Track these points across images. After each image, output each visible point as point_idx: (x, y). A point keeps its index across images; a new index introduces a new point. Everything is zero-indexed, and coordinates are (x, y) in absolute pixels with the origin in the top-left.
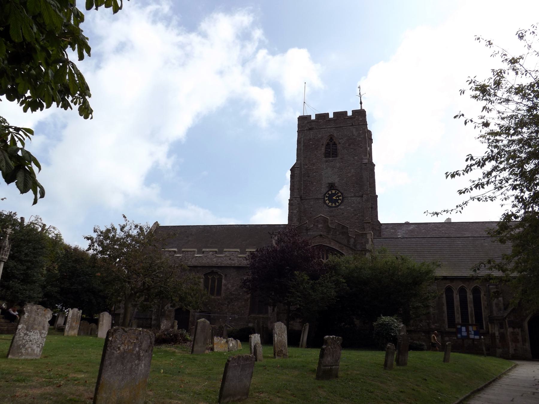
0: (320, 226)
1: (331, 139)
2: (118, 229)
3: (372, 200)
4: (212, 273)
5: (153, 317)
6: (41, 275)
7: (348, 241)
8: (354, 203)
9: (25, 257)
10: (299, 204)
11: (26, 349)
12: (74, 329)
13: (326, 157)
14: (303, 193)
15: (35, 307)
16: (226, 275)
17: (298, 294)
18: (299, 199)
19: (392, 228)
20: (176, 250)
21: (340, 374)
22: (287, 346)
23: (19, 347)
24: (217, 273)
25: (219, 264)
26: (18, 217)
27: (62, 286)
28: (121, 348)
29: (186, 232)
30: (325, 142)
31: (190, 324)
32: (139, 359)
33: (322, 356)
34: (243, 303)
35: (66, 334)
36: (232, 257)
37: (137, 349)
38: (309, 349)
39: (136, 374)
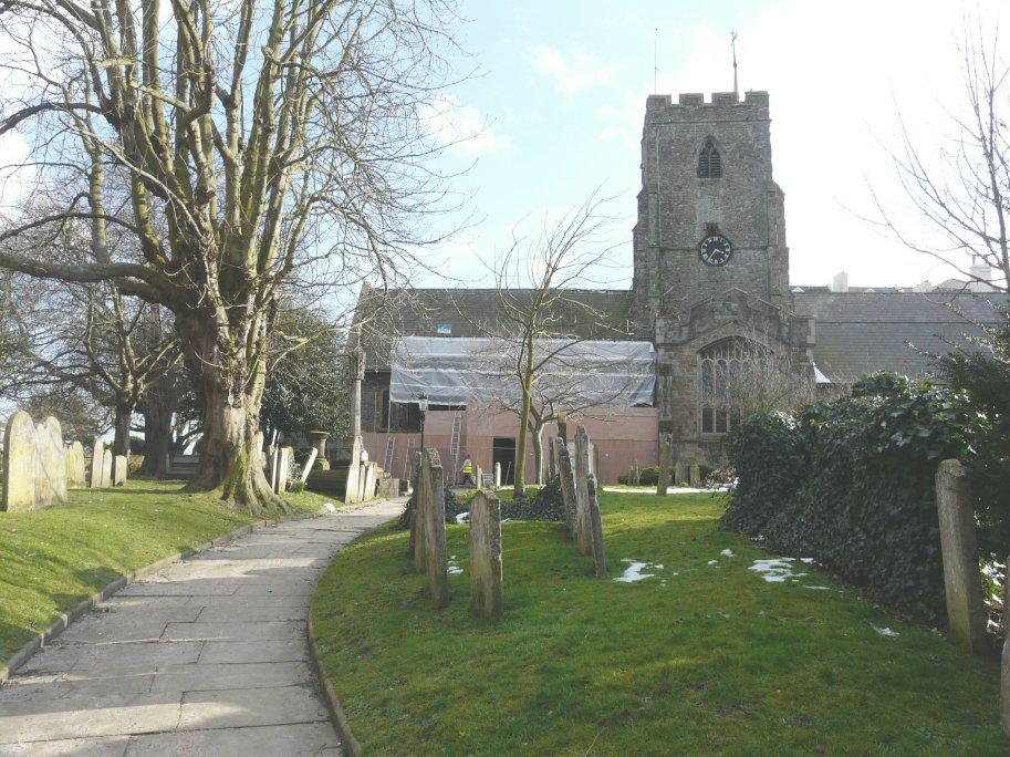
0: (733, 305)
1: (710, 141)
3: (782, 255)
7: (779, 331)
13: (700, 176)
30: (699, 147)
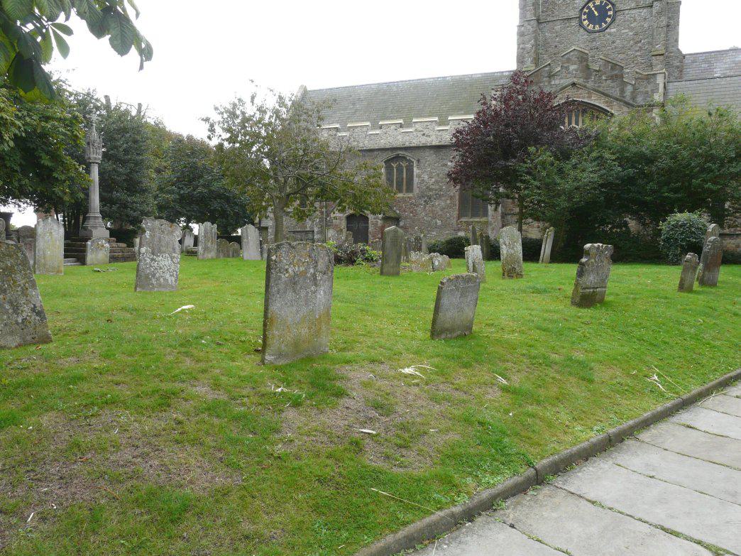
0: (572, 67)
2: (247, 100)
4: (397, 158)
5: (316, 230)
6: (151, 180)
7: (622, 91)
8: (635, 20)
9: (125, 155)
10: (535, 32)
11: (158, 279)
12: (210, 251)
14: (542, 12)
15: (157, 222)
16: (418, 161)
17: (537, 183)
18: (534, 23)
19: (705, 61)
20: (338, 126)
21: (607, 298)
22: (522, 261)
23: (148, 277)
24: (404, 158)
25: (407, 144)
26: (100, 95)
27: (182, 192)
28: (290, 270)
29: (351, 96)
31: (370, 236)
32: (316, 285)
33: (580, 274)
34: (448, 202)
35: (200, 257)
36: (426, 132)
37: (312, 271)
38: (555, 265)
39: (315, 304)
